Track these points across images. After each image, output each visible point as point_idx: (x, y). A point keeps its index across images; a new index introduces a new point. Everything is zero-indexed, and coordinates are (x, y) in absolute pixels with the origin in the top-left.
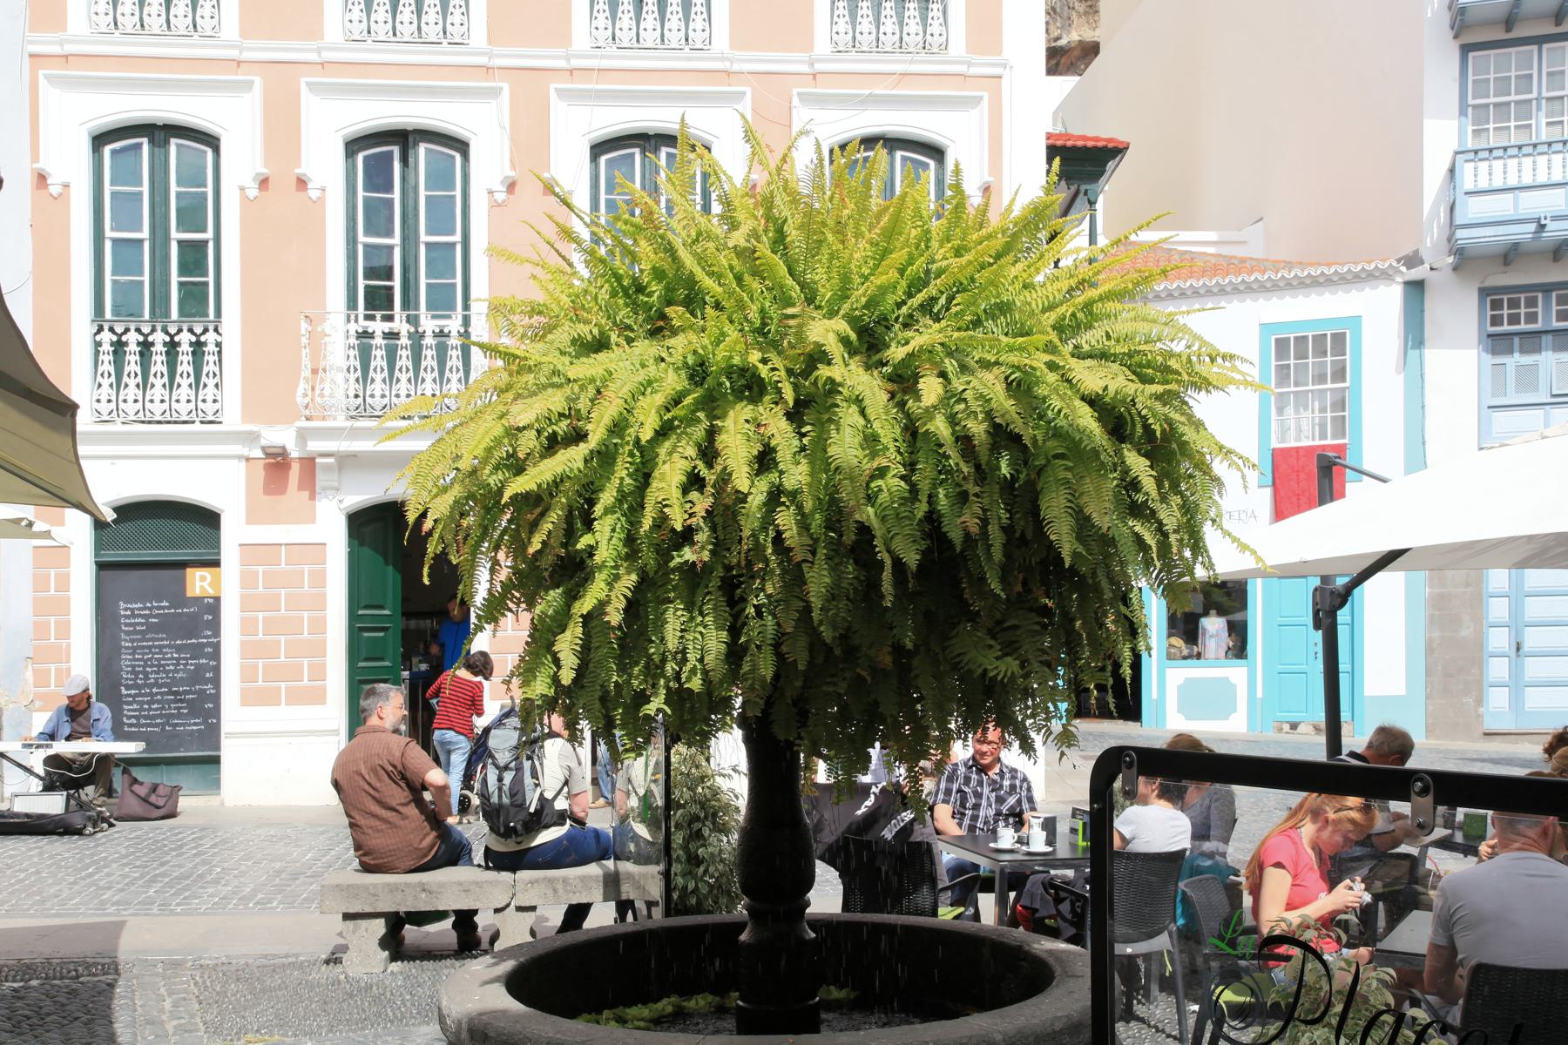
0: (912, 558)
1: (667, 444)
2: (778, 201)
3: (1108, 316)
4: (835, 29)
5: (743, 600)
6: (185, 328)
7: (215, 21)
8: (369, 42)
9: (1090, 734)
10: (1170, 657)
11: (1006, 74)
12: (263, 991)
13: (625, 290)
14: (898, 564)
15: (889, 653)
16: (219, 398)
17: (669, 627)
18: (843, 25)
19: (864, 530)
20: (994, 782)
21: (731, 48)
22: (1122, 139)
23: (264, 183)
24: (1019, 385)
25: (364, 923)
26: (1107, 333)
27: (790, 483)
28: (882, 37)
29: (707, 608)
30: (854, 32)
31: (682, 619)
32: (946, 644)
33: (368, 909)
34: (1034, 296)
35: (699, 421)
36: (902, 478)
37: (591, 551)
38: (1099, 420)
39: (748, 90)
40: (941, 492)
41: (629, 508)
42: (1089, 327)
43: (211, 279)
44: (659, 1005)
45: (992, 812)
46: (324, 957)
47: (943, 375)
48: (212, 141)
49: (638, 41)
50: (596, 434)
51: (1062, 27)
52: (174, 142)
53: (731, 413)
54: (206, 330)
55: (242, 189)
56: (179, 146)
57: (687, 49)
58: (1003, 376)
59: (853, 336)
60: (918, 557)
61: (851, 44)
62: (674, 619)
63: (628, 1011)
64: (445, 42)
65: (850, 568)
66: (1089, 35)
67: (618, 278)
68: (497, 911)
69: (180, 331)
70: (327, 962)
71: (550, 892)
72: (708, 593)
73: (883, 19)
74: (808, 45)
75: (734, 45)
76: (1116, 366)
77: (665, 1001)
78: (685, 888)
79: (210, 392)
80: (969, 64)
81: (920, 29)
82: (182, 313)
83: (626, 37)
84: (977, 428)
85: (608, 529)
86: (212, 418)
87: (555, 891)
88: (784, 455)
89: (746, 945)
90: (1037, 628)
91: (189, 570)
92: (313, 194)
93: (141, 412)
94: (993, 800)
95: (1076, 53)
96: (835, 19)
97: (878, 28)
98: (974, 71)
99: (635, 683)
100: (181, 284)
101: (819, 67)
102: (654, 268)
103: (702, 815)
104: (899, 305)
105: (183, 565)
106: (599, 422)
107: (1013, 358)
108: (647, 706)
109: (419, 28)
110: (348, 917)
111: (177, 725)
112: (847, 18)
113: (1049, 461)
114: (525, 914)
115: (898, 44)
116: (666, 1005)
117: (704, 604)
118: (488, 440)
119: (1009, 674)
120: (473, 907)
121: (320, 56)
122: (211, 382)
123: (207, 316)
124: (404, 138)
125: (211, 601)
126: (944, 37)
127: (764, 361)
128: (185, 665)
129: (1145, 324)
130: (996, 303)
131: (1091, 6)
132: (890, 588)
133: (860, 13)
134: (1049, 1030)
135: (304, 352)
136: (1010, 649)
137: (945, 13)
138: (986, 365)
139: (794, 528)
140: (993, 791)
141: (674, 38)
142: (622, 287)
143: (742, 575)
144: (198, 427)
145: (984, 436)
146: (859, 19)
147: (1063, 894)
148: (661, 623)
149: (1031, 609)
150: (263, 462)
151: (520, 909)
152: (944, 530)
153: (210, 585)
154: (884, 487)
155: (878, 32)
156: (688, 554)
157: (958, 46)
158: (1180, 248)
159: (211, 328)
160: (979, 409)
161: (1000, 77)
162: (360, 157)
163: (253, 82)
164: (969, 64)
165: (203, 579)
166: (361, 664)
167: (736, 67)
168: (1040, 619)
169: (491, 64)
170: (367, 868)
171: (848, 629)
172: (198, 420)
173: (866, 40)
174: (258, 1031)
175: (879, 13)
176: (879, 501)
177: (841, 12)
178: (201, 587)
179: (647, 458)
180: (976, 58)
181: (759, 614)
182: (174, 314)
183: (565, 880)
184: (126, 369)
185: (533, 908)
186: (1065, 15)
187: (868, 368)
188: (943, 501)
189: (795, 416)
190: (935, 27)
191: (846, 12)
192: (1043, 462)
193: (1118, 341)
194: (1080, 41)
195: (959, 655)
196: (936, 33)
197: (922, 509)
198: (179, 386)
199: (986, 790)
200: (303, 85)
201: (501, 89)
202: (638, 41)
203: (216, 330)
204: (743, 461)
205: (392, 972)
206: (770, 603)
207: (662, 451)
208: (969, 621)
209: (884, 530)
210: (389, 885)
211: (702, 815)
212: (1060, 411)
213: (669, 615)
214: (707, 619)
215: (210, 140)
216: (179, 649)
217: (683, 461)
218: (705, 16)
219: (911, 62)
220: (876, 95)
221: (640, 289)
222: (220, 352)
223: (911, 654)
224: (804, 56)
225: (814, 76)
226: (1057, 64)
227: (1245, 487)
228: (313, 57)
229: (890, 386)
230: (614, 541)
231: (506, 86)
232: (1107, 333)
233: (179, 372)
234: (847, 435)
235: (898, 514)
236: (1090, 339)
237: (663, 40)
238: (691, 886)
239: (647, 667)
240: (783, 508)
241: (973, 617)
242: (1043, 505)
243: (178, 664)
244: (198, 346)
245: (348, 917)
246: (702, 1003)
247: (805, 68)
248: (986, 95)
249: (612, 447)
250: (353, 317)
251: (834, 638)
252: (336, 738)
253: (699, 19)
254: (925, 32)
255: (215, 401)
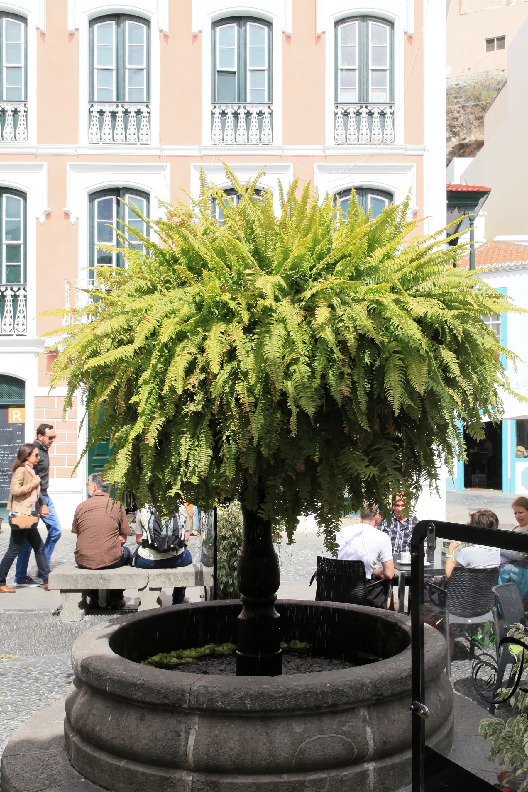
0: (310, 410)
1: (181, 345)
2: (249, 211)
3: (435, 274)
4: (336, 133)
5: (220, 432)
6: (9, 288)
7: (25, 135)
8: (101, 144)
9: (475, 496)
10: (517, 456)
11: (425, 154)
12: (17, 629)
13: (168, 262)
14: (302, 414)
15: (303, 463)
16: (25, 323)
17: (182, 447)
18: (340, 131)
19: (284, 394)
20: (404, 526)
21: (283, 144)
22: (487, 187)
23: (48, 215)
24: (374, 310)
25: (71, 595)
26: (434, 283)
27: (243, 368)
28: (361, 136)
29: (202, 436)
30: (346, 134)
31: (190, 443)
32: (338, 458)
33: (73, 588)
34: (393, 263)
35: (198, 332)
36: (308, 364)
37: (137, 404)
38: (423, 331)
39: (291, 165)
40: (331, 373)
41: (160, 381)
42: (424, 280)
43: (22, 264)
44: (202, 649)
45: (401, 542)
46: (53, 611)
47: (331, 307)
48: (22, 194)
49: (236, 141)
50: (139, 341)
51: (467, 134)
52: (5, 196)
53: (214, 327)
54: (19, 289)
55: (37, 218)
56: (7, 198)
57: (260, 144)
58: (366, 307)
59: (284, 285)
60: (314, 410)
61: (345, 140)
62: (185, 442)
63: (184, 652)
64: (139, 143)
65: (279, 415)
66: (480, 137)
67: (164, 255)
68: (140, 590)
69: (6, 289)
70: (53, 614)
71: (167, 581)
72: (203, 428)
73: (361, 127)
74: (323, 142)
75: (284, 142)
76: (434, 301)
77: (206, 647)
78: (227, 583)
79: (20, 320)
80: (406, 149)
81: (381, 132)
82: (8, 280)
83: (229, 139)
84: (350, 337)
85: (147, 393)
86: (22, 333)
87: (170, 580)
88: (241, 352)
89: (242, 621)
90: (392, 449)
91: (10, 410)
92: (72, 220)
93: (13, 330)
94: (403, 535)
95: (474, 146)
96: (337, 127)
97: (359, 132)
98: (409, 153)
99: (167, 478)
100: (8, 266)
101: (328, 152)
102: (182, 250)
103: (237, 544)
104: (311, 269)
105: (7, 407)
106: (142, 332)
107: (371, 297)
108: (170, 491)
109: (126, 137)
110: (62, 591)
111: (3, 487)
112: (343, 127)
113: (391, 355)
114: (154, 592)
115: (369, 140)
116: (206, 649)
117: (200, 434)
118: (84, 341)
119: (371, 476)
120: (123, 588)
121: (76, 151)
122: (21, 315)
123: (20, 282)
124: (117, 191)
125: (21, 425)
126: (393, 136)
127: (233, 299)
128: (7, 457)
129: (455, 278)
130: (369, 267)
131: (481, 122)
132: (295, 426)
133: (349, 124)
134: (399, 677)
135: (66, 300)
136: (373, 462)
137: (393, 123)
138: (359, 301)
139: (246, 393)
140: (402, 530)
141: (254, 138)
142: (166, 260)
143: (221, 419)
144: (14, 338)
145: (353, 341)
146: (349, 127)
147: (434, 590)
148: (178, 445)
149: (390, 439)
150: (46, 355)
151: (151, 589)
152: (331, 394)
153: (19, 417)
154: (297, 370)
155: (359, 134)
156: (192, 407)
157: (400, 140)
158: (523, 244)
159: (22, 288)
160: (351, 326)
161: (422, 156)
162: (96, 202)
163: (43, 165)
164: (406, 149)
165: (17, 414)
166: (95, 457)
167: (285, 153)
168: (393, 444)
169: (161, 154)
170: (81, 567)
171: (278, 450)
172: (15, 334)
173: (352, 138)
174: (8, 652)
175: (359, 124)
176: (294, 378)
177: (340, 124)
178: (16, 418)
179: (171, 353)
180: (410, 146)
181: (228, 441)
182: (4, 281)
183: (175, 575)
184: (19, 309)
185: (160, 589)
186: (468, 127)
187: (293, 302)
188: (332, 378)
189: (248, 330)
190: (388, 131)
191: (342, 124)
192: (388, 355)
193: (440, 287)
194: (476, 140)
195: (345, 464)
196: (389, 133)
197: (317, 382)
198: (18, 317)
199: (399, 530)
200: (68, 167)
201: (166, 166)
202: (236, 141)
203: (24, 289)
204: (216, 355)
205: (85, 621)
206: (234, 435)
207: (178, 349)
208: (351, 445)
209: (295, 394)
210: (84, 575)
211: (237, 544)
212: (398, 325)
213: (183, 441)
214: (201, 443)
215: (22, 194)
216: (5, 449)
217: (188, 356)
218: (270, 127)
219: (376, 149)
220: (358, 166)
221: (176, 261)
222: (26, 300)
223: (316, 465)
224: (321, 147)
225: (326, 157)
226: (464, 152)
227: (516, 369)
228: (73, 152)
229: (304, 313)
230: (151, 400)
231: (168, 165)
232: (434, 283)
233: (6, 310)
234: (274, 340)
235: (304, 385)
236: (425, 286)
237: (248, 140)
238: (230, 582)
239: (172, 469)
240: (240, 381)
241: (354, 443)
242: (386, 380)
243: (4, 457)
244: (15, 297)
245: (62, 591)
246: (226, 648)
247: (321, 153)
248: (415, 165)
249: (152, 346)
250: (91, 282)
251: (270, 455)
252: (81, 495)
253: (267, 129)
254: (383, 133)
255: (23, 325)
